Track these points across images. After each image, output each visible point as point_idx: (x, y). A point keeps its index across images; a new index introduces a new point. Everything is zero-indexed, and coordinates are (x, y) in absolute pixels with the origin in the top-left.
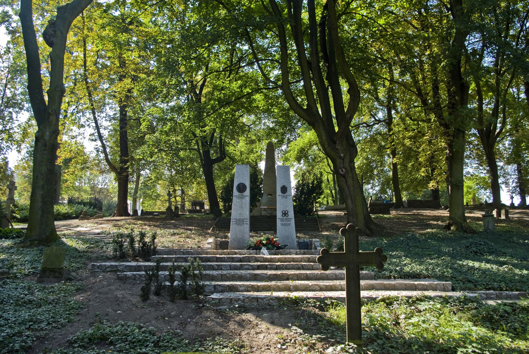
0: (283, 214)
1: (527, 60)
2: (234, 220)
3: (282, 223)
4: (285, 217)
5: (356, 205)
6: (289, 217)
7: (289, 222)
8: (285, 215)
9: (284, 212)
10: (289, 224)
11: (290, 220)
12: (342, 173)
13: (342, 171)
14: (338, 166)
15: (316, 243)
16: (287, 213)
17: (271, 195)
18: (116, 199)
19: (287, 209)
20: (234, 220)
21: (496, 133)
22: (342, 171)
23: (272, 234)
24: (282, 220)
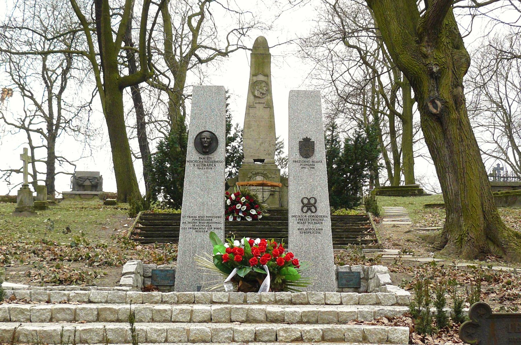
0: (304, 205)
1: (422, 6)
2: (188, 220)
3: (300, 226)
4: (309, 213)
5: (465, 186)
6: (319, 213)
7: (318, 226)
8: (309, 209)
9: (305, 201)
10: (319, 231)
11: (319, 220)
12: (434, 111)
13: (436, 107)
14: (426, 96)
15: (380, 276)
16: (314, 205)
17: (262, 161)
18: (440, 191)
19: (315, 194)
20: (188, 220)
21: (412, 89)
22: (436, 107)
23: (340, 270)
24: (301, 221)
